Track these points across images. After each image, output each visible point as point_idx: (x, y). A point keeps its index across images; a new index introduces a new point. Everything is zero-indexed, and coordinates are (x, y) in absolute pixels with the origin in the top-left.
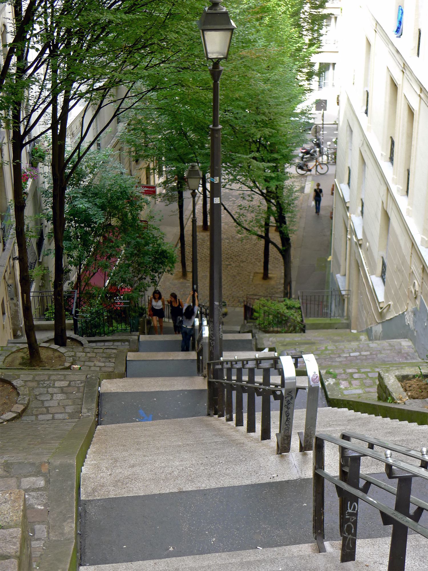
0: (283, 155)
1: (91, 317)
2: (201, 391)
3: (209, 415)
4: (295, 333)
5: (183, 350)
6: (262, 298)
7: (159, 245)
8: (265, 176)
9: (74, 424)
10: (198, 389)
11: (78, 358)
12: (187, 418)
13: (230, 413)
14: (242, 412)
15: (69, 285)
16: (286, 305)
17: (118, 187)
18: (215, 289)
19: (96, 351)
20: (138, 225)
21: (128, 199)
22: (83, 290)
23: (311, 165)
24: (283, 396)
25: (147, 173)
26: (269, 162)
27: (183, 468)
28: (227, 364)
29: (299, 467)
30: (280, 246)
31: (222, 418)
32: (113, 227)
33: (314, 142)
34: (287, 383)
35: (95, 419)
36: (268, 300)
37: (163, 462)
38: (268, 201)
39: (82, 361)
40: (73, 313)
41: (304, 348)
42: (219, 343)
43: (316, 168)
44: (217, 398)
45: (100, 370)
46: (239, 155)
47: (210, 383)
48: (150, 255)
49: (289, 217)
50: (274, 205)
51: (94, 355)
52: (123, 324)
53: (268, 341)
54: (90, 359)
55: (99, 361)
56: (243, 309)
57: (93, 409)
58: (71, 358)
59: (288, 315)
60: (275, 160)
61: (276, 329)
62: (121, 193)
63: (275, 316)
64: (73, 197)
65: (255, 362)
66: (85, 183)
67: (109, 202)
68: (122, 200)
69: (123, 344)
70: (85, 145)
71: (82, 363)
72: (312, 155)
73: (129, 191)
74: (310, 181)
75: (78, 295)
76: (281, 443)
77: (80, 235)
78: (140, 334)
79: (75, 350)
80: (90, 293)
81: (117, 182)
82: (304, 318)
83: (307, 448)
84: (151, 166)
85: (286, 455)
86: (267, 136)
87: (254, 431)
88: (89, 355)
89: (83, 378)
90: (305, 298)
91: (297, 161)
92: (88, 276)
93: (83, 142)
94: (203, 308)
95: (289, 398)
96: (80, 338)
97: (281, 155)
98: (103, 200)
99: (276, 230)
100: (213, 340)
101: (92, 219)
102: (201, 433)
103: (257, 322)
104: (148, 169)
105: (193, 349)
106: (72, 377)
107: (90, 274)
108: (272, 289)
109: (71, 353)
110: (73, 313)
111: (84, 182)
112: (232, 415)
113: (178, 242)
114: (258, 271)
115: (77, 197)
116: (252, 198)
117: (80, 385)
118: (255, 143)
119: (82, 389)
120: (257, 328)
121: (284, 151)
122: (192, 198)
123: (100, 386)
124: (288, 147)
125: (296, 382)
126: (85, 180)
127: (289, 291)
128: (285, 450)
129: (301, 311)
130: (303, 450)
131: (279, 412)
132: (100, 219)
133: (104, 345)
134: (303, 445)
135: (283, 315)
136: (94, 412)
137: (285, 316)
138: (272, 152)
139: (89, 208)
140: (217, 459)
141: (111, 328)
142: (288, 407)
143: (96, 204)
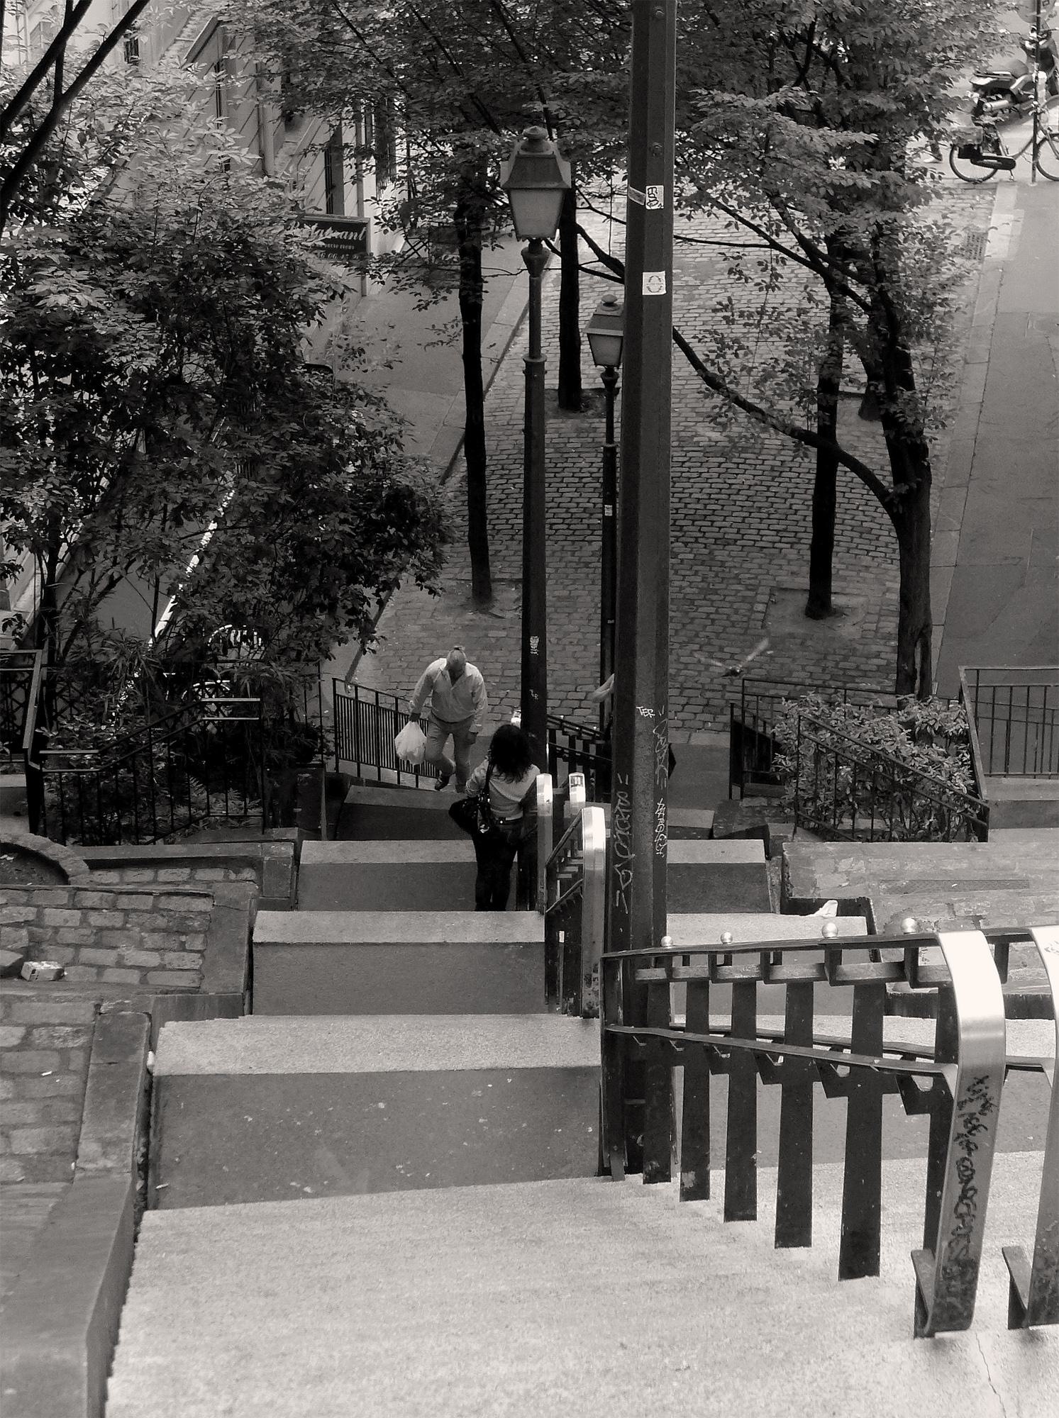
0: (907, 100)
1: (98, 762)
2: (573, 1074)
3: (604, 1171)
4: (945, 839)
5: (483, 904)
6: (811, 696)
7: (384, 466)
8: (832, 185)
9: (51, 1203)
10: (560, 1064)
11: (50, 932)
12: (514, 1186)
13: (697, 1162)
14: (754, 1162)
15: (4, 628)
16: (910, 724)
17: (214, 225)
18: (638, 650)
19: (124, 902)
20: (296, 384)
21: (257, 272)
22: (66, 650)
23: (1014, 139)
24: (951, 1100)
25: (328, 170)
26: (844, 125)
27: (530, 1386)
28: (686, 962)
29: (1009, 1390)
30: (886, 480)
31: (660, 1186)
32: (192, 393)
33: (1027, 44)
34: (968, 1042)
35: (134, 1183)
36: (831, 704)
37: (444, 1364)
38: (837, 289)
39: (68, 945)
40: (27, 744)
41: (986, 904)
42: (651, 880)
43: (1035, 154)
44: (643, 1102)
45: (143, 981)
46: (727, 97)
47: (610, 1042)
48: (344, 511)
49: (925, 358)
50: (863, 305)
51: (117, 920)
52: (232, 793)
53: (836, 870)
54: (100, 938)
55: (140, 945)
56: (725, 740)
57: (126, 1141)
58: (24, 932)
59: (919, 763)
60: (872, 119)
61: (863, 823)
62: (228, 247)
63: (858, 769)
64: (27, 261)
65: (756, 958)
66: (71, 204)
67: (176, 286)
68: (230, 277)
69: (233, 876)
70: (81, 44)
71: (69, 953)
72: (1016, 99)
73: (260, 237)
74: (1008, 211)
75: (45, 670)
76: (937, 1294)
77: (56, 423)
78: (303, 836)
79: (39, 898)
80: (94, 665)
81: (209, 200)
82: (982, 780)
83: (1043, 1314)
84: (348, 136)
85: (952, 1342)
86: (843, 18)
87: (806, 1242)
88: (95, 919)
89: (84, 1014)
90: (986, 695)
91: (958, 122)
92: (87, 590)
93: (76, 31)
94: (559, 733)
95: (975, 1107)
96: (54, 850)
97: (896, 99)
98: (152, 278)
99: (866, 413)
100: (627, 866)
101: (108, 356)
102: (582, 1246)
103: (790, 791)
104: (333, 151)
105: (526, 900)
106: (38, 1011)
107: (93, 585)
108: (846, 658)
109: (22, 909)
110: (27, 744)
111: (72, 198)
112: (708, 1173)
113: (455, 458)
114: (787, 581)
115: (46, 262)
116: (776, 276)
117: (70, 1044)
118: (790, 45)
119: (77, 1061)
120: (786, 820)
121: (911, 81)
122: (526, 274)
123: (152, 1046)
124: (928, 65)
125: (1003, 1041)
126: (73, 191)
127: (918, 667)
128: (952, 1318)
129: (971, 752)
130: (1024, 1323)
131: (924, 1162)
132: (139, 357)
133: (155, 881)
134: (1026, 1303)
135: (895, 765)
136: (131, 1152)
137: (904, 771)
138: (860, 84)
139: (98, 309)
140: (664, 1354)
141: (182, 811)
142: (968, 1142)
143: (121, 294)
